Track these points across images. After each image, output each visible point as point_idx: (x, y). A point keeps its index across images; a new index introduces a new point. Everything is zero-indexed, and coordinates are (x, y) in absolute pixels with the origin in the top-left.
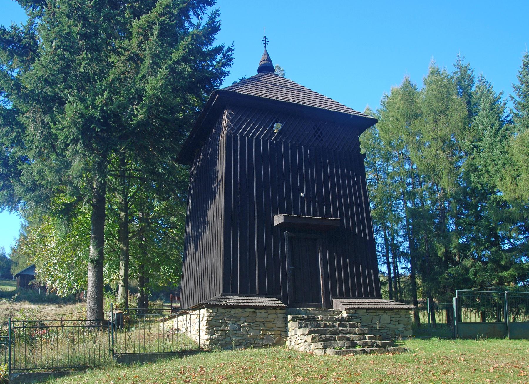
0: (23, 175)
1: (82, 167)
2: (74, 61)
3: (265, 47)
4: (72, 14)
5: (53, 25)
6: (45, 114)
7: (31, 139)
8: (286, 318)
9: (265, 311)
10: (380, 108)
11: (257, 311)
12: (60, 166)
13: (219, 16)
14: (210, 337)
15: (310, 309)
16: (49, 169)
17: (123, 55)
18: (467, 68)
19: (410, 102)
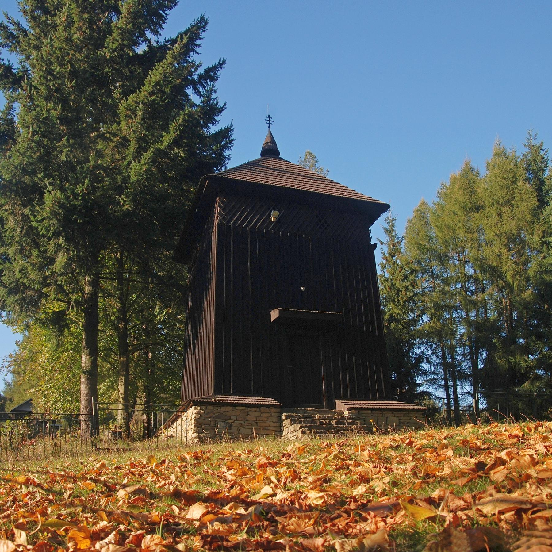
0: (4, 275)
1: (65, 262)
2: (54, 148)
3: (269, 127)
4: (51, 97)
5: (30, 109)
6: (25, 206)
7: (11, 235)
8: (281, 417)
9: (258, 409)
10: (437, 200)
11: (249, 409)
12: (43, 262)
13: (215, 92)
14: (198, 435)
15: (309, 409)
16: (31, 266)
17: (112, 141)
18: (540, 148)
19: (471, 191)
